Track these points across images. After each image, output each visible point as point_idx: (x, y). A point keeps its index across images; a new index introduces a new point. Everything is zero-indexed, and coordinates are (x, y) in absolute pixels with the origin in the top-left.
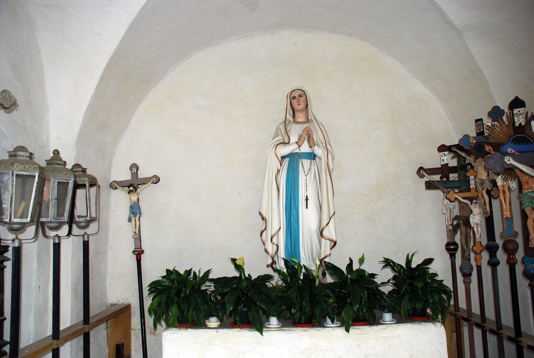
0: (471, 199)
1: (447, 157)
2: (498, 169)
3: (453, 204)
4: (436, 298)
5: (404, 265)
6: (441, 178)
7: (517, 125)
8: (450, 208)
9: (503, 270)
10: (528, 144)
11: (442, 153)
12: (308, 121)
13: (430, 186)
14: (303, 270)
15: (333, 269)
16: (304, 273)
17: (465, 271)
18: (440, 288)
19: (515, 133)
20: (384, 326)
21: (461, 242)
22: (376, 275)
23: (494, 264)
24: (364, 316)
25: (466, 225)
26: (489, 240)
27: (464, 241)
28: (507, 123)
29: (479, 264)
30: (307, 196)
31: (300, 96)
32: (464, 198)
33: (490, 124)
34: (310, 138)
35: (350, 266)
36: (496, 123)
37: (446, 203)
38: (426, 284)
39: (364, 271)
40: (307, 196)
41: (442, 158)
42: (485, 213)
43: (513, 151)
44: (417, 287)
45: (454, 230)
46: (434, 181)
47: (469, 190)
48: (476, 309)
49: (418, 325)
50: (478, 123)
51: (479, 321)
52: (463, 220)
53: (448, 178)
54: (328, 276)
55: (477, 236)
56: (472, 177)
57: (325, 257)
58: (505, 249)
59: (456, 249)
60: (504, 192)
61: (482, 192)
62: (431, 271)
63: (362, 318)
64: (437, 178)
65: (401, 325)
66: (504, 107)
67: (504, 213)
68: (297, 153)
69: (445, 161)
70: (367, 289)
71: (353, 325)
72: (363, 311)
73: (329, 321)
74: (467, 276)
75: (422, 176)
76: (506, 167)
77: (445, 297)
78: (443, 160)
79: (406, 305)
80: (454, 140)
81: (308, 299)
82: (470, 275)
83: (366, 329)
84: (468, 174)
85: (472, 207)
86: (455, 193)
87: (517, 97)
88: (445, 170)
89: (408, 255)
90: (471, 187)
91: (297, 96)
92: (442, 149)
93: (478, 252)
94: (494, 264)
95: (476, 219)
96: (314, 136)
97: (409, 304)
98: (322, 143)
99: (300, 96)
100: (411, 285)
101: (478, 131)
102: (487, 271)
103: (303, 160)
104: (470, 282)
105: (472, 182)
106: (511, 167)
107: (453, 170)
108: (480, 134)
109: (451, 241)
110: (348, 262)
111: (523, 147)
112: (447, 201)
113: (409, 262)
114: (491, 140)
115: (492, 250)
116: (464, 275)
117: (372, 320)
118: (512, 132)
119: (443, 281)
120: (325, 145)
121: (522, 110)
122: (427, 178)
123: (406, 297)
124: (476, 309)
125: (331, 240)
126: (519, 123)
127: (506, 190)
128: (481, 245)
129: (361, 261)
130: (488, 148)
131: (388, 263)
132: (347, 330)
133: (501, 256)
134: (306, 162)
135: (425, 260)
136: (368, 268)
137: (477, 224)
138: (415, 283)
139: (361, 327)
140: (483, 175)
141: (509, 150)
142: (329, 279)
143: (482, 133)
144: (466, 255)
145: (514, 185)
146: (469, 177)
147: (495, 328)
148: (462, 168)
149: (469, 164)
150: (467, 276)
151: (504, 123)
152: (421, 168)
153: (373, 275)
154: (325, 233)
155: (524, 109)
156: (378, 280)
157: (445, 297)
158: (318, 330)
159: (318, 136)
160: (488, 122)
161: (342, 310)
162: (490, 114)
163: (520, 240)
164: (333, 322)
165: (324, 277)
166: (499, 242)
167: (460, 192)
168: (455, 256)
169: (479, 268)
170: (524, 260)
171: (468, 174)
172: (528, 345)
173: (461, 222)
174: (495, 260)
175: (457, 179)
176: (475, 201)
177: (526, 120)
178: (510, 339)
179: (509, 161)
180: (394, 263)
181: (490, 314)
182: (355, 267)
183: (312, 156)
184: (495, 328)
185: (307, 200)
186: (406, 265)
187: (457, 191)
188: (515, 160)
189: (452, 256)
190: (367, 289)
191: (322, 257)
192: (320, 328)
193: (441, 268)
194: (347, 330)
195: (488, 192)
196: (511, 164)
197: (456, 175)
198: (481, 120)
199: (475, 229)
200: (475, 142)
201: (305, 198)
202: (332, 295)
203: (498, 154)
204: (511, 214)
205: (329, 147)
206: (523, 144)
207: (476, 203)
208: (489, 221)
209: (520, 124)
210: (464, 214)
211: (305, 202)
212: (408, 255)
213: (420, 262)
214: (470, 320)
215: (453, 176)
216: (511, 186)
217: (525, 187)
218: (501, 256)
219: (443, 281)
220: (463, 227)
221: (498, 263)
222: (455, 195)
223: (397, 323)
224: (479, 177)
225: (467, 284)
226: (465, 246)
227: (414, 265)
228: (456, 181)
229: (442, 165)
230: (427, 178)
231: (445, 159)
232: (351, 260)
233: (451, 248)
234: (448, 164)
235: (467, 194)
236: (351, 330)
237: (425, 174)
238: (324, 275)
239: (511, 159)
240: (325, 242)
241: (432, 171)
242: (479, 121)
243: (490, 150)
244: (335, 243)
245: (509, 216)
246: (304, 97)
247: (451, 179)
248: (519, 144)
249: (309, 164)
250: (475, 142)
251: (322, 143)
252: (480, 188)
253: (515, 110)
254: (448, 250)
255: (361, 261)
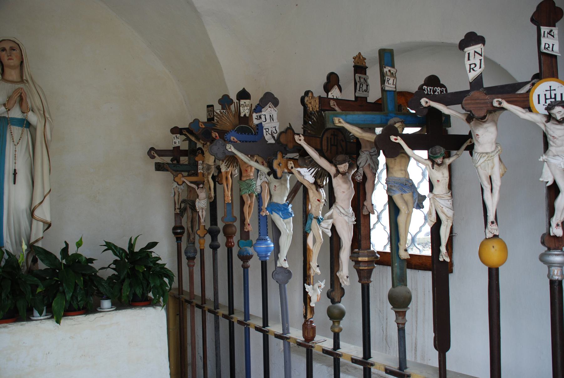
0: (197, 184)
1: (179, 140)
2: (220, 156)
3: (182, 186)
4: (158, 283)
5: (126, 248)
6: (172, 160)
7: (242, 115)
8: (178, 192)
9: (222, 252)
10: (248, 134)
11: (174, 135)
12: (22, 81)
13: (159, 167)
14: (6, 256)
15: (47, 255)
16: (7, 261)
17: (189, 254)
18: (163, 272)
19: (240, 123)
20: (101, 314)
21: (187, 224)
22: (95, 260)
23: (214, 247)
24: (78, 305)
25: (192, 210)
26: (211, 225)
27: (190, 225)
28: (234, 112)
29: (202, 248)
30: (15, 170)
31: (12, 49)
32: (191, 182)
33: (218, 111)
34: (21, 100)
35: (65, 251)
36: (225, 111)
37: (175, 187)
38: (149, 268)
39: (80, 255)
40: (15, 170)
41: (174, 141)
42: (209, 197)
43: (236, 140)
44: (138, 271)
45: (179, 215)
46: (163, 164)
47: (196, 174)
48: (197, 291)
49: (138, 311)
50: (210, 109)
51: (199, 303)
52: (190, 204)
53: (178, 161)
54: (39, 261)
55: (202, 220)
56: (200, 162)
57: (37, 241)
58: (225, 234)
59: (182, 233)
60: (227, 178)
61: (208, 178)
62: (154, 255)
63: (76, 307)
64: (168, 160)
65: (120, 311)
66: (233, 96)
67: (226, 199)
68: (5, 117)
69: (177, 143)
70: (84, 275)
71: (65, 315)
72: (77, 299)
73: (36, 313)
74: (191, 259)
75: (153, 157)
76: (227, 154)
77: (166, 280)
78: (175, 143)
79: (126, 292)
80: (184, 124)
81: (9, 290)
82: (194, 258)
83: (81, 318)
84: (197, 159)
85: (198, 191)
86: (183, 176)
87: (244, 88)
88: (176, 152)
89: (131, 239)
90: (199, 171)
91: (8, 48)
92: (175, 131)
93: (202, 236)
94: (214, 247)
95: (202, 204)
96: (28, 101)
97: (129, 290)
98: (39, 110)
99: (12, 49)
100: (133, 269)
101: (209, 117)
102: (208, 252)
103: (12, 127)
104: (194, 266)
105: (200, 167)
106: (232, 154)
107: (185, 153)
108: (210, 120)
109: (178, 224)
110: (64, 246)
111: (245, 137)
112: (176, 184)
113: (131, 246)
114: (218, 127)
115: (214, 234)
116: (188, 258)
117: (90, 308)
118: (238, 122)
119: (165, 264)
120: (42, 112)
121: (247, 101)
122: (158, 159)
123: (127, 283)
124: (197, 291)
125: (44, 222)
126: (244, 114)
127: (229, 176)
128: (205, 229)
129: (79, 244)
130: (215, 134)
131: (109, 246)
132: (58, 322)
133: (221, 239)
134: (16, 130)
135: (149, 244)
136: (85, 252)
137: (202, 209)
138: (137, 268)
139: (76, 317)
140: (210, 160)
141: (232, 138)
142: (42, 266)
143: (213, 119)
144: (191, 238)
145: (236, 172)
146: (198, 162)
147: (212, 308)
148: (193, 152)
149: (200, 149)
150: (191, 259)
151: (231, 112)
152: (152, 149)
153: (91, 260)
154: (37, 213)
155: (249, 101)
156: (96, 265)
157: (166, 280)
158: (22, 325)
159: (34, 100)
160: (218, 108)
161: (53, 300)
162: (221, 102)
163: (237, 224)
164: (41, 314)
165: (34, 264)
166: (220, 225)
167: (189, 175)
168: (181, 240)
169: (202, 251)
170: (240, 243)
171: (197, 159)
172: (238, 321)
173: (188, 206)
174: (216, 243)
175: (187, 163)
176: (201, 186)
177: (250, 112)
178: (224, 316)
179: (231, 148)
180: (115, 247)
181: (209, 294)
182: (71, 251)
183: (26, 124)
184: (212, 308)
185: (15, 174)
186: (129, 249)
187: (185, 174)
188: (235, 148)
189: (179, 239)
190: (84, 275)
191: (32, 240)
192: (24, 323)
193: (165, 253)
194: (58, 322)
195: (214, 178)
196: (232, 152)
197: (187, 158)
198: (212, 106)
199: (200, 214)
200: (203, 126)
201: (12, 172)
202: (40, 284)
203: (221, 142)
204: (232, 200)
205: (47, 115)
206: (245, 134)
207: (202, 188)
208: (213, 206)
209: (245, 115)
210: (191, 199)
211: (12, 177)
212: (131, 239)
213: (144, 245)
214: (192, 302)
215: (184, 160)
216: (233, 173)
217: (244, 174)
218: (221, 239)
219: (165, 264)
220: (189, 211)
221: (218, 247)
222: (183, 179)
223: (116, 310)
224: (206, 162)
225: (191, 267)
226: (190, 230)
227: (137, 249)
228: (186, 165)
229: (174, 148)
230: (158, 159)
231: (177, 142)
232: (67, 245)
233: (178, 232)
234: (179, 147)
235: (194, 179)
236: (62, 321)
237: (156, 155)
238: (35, 261)
239: (232, 147)
240: (37, 224)
241: (162, 153)
242: (210, 107)
243: (216, 137)
244: (50, 225)
245: (230, 202)
246: (18, 51)
247: (181, 162)
248: (241, 133)
249: (21, 132)
250: (203, 126)
251: (39, 110)
252: (206, 174)
253: (242, 101)
254: (175, 233)
255: (79, 244)
